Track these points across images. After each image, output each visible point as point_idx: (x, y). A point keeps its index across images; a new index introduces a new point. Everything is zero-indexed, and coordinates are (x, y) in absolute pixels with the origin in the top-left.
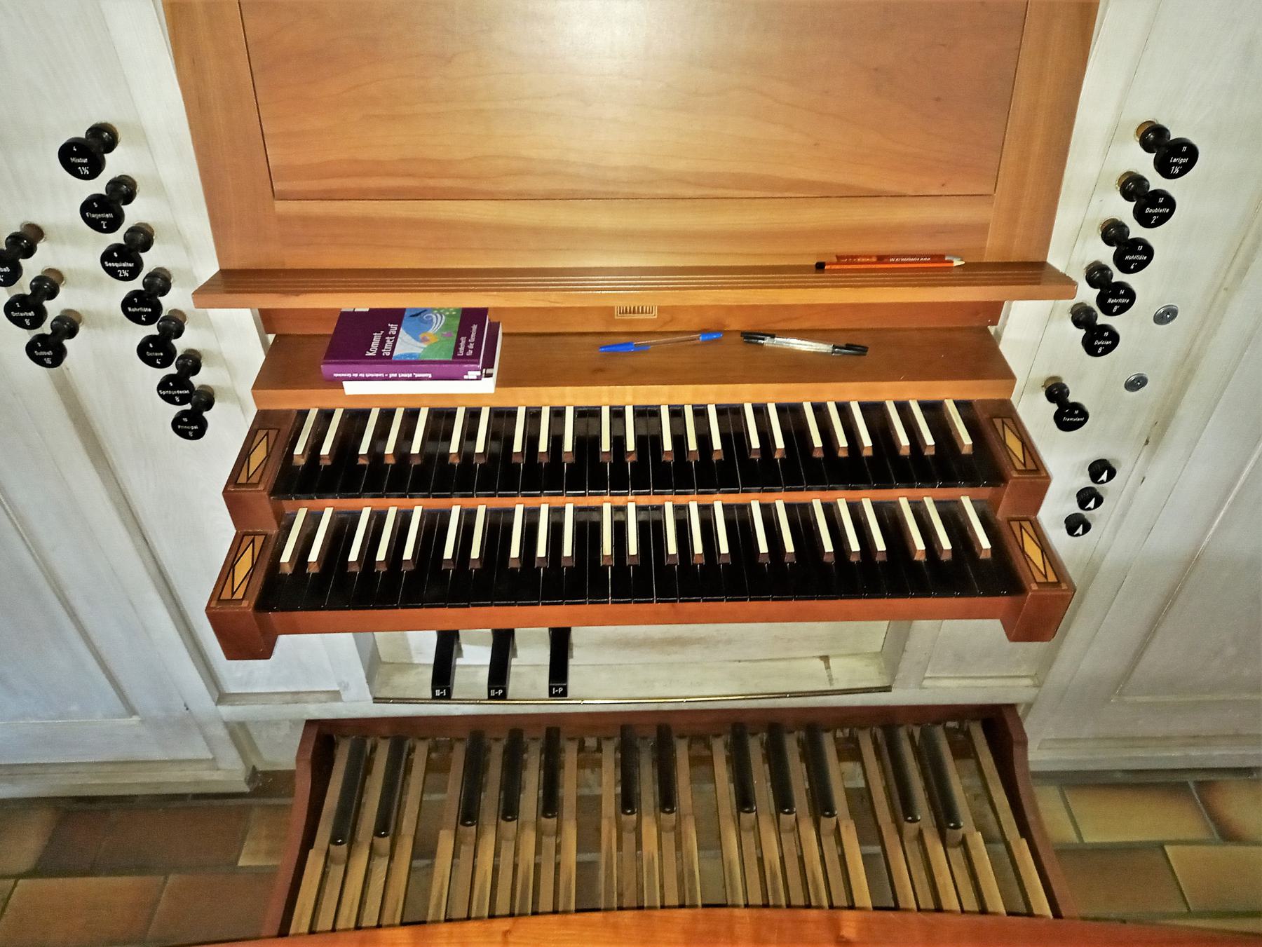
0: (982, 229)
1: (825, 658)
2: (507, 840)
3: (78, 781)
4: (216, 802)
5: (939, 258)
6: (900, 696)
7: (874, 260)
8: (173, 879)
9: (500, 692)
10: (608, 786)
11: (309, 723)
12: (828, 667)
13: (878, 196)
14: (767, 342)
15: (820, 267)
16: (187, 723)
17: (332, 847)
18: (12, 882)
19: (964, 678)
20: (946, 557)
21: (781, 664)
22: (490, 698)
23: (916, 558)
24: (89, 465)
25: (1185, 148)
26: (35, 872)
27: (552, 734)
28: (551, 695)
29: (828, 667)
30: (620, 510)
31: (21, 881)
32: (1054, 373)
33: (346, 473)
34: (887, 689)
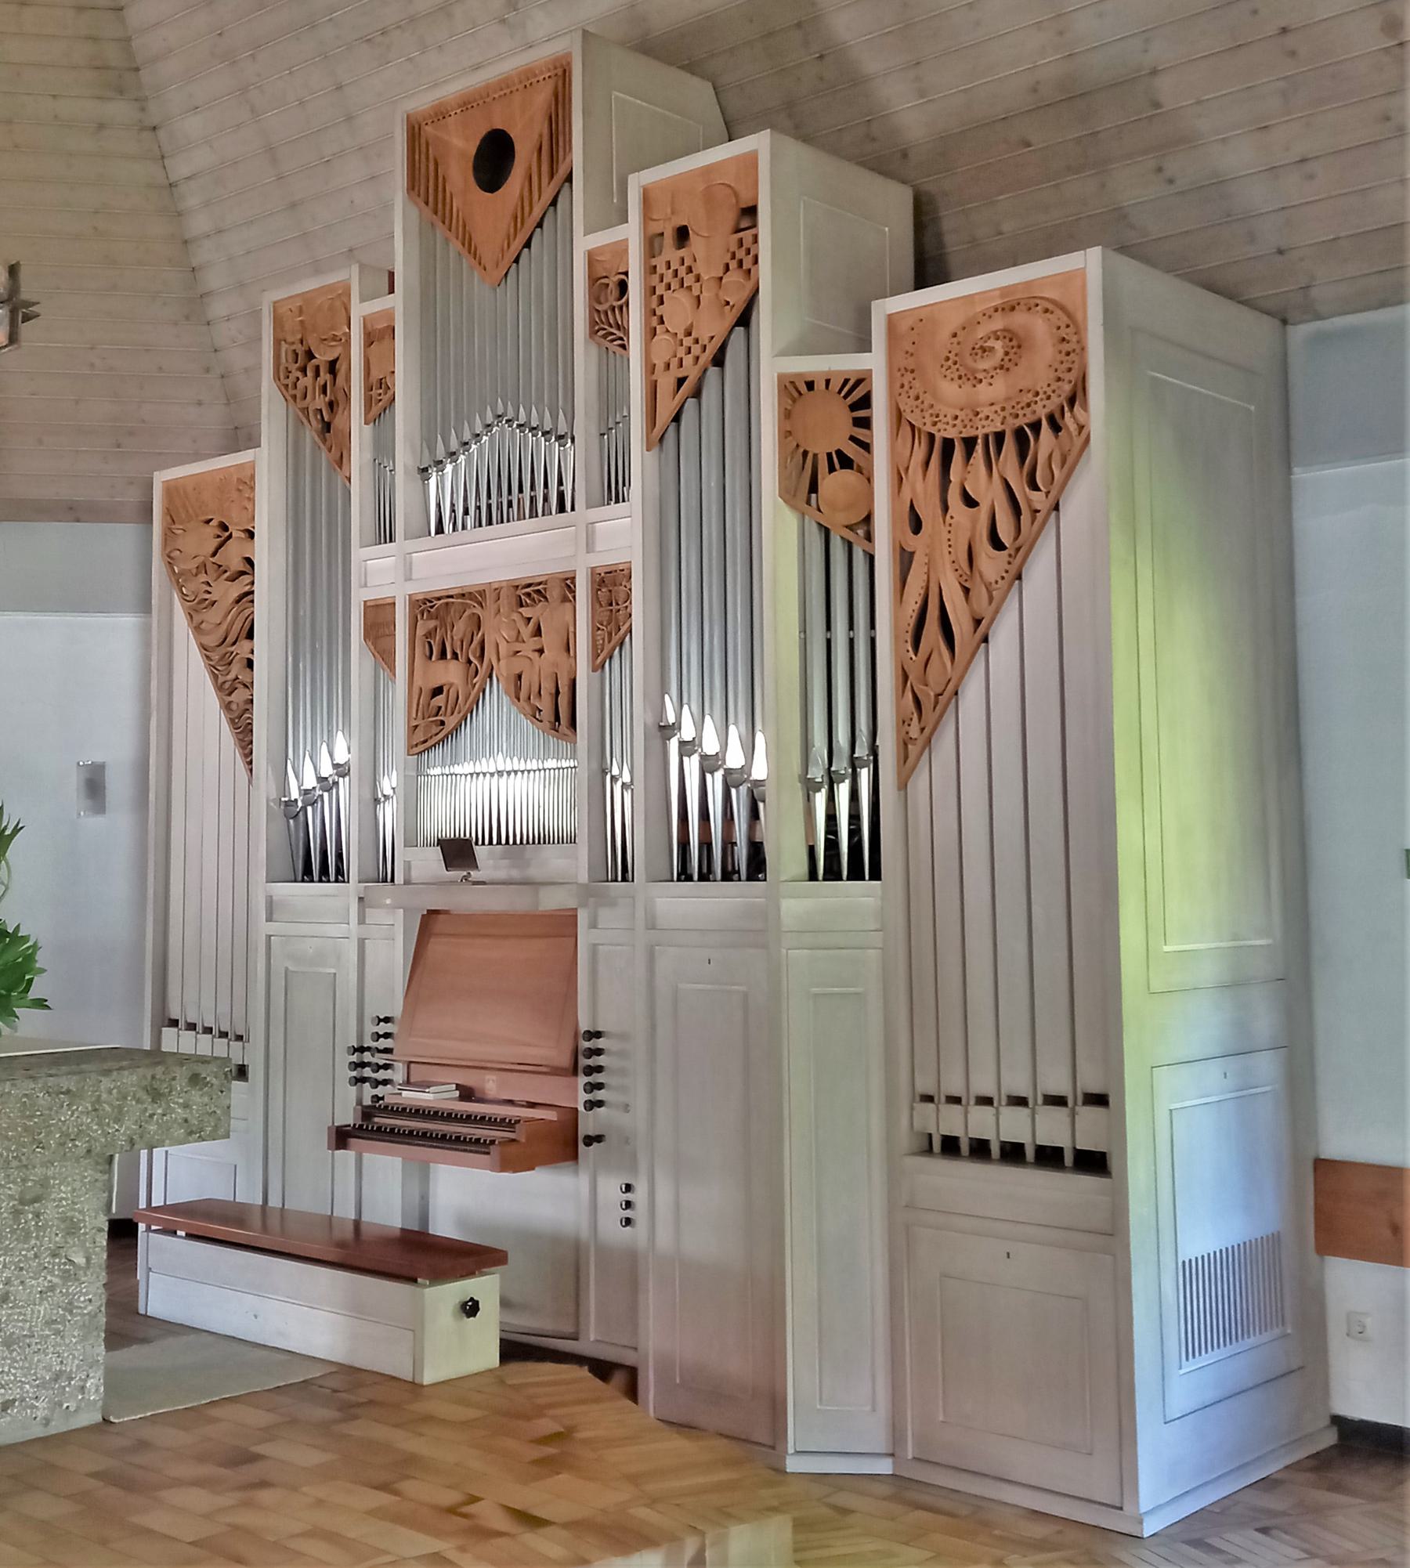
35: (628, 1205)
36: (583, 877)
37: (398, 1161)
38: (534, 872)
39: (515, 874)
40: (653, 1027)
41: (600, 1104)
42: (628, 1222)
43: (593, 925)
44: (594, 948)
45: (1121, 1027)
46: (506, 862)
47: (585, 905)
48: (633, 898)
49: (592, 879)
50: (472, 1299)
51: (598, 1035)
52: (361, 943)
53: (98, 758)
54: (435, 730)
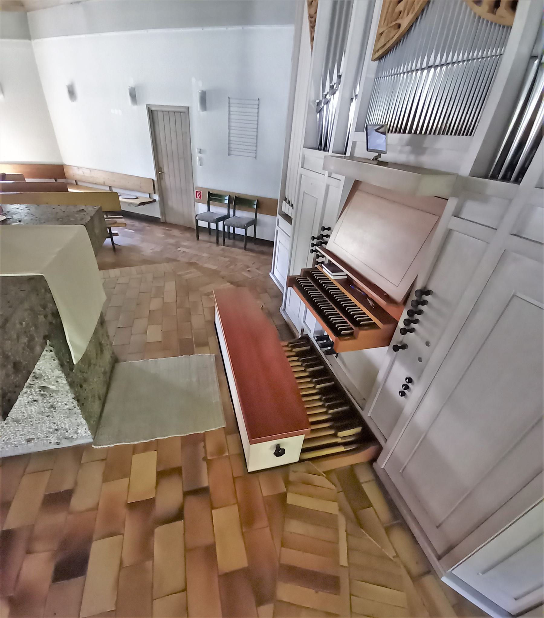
35: (407, 387)
36: (465, 169)
37: (122, 209)
38: (427, 160)
39: (411, 159)
40: (474, 311)
41: (412, 330)
42: (403, 394)
43: (457, 214)
44: (449, 233)
45: (51, 123)
46: (408, 148)
47: (455, 194)
48: (511, 200)
49: (473, 174)
50: (284, 450)
51: (428, 293)
52: (328, 187)
53: (331, 237)
54: (393, 32)
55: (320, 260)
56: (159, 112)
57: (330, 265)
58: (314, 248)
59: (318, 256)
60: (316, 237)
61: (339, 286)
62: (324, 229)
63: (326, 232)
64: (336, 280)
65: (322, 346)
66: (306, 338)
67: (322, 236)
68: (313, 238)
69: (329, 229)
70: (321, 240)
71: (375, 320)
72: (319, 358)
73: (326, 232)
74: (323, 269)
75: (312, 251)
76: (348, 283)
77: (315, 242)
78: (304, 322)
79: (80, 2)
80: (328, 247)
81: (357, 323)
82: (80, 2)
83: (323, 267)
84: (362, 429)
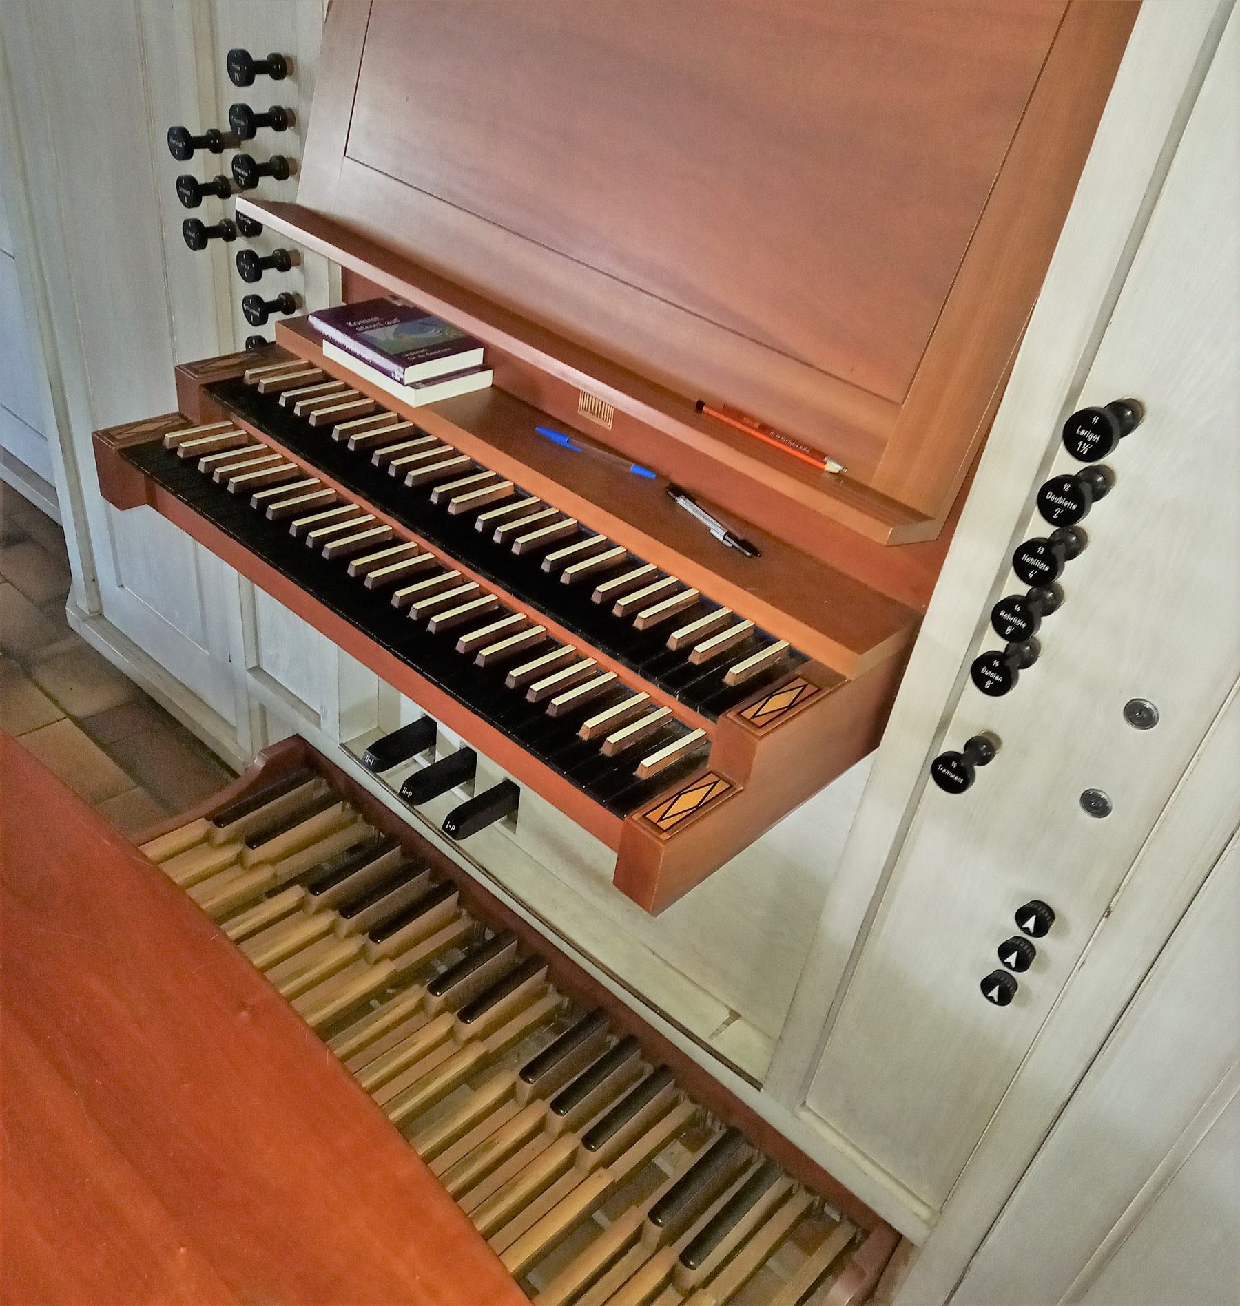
0: (879, 444)
1: (735, 1015)
2: (456, 1042)
3: (155, 682)
4: (219, 769)
5: (820, 455)
6: (767, 1105)
7: (757, 425)
8: (140, 790)
9: (453, 828)
10: (677, 1163)
11: (298, 737)
12: (727, 1023)
13: (811, 366)
14: (682, 501)
15: (700, 405)
16: (231, 682)
17: (649, 1223)
18: (63, 716)
19: (846, 1140)
20: (550, 712)
21: (686, 986)
22: (401, 795)
23: (579, 733)
24: (647, 683)
25: (1096, 420)
26: (78, 722)
27: (448, 881)
28: (444, 827)
29: (727, 1023)
30: (365, 517)
31: (67, 720)
32: (1001, 735)
33: (265, 410)
34: (757, 1085)
55: (271, 285)
56: (437, 1173)
57: (357, 313)
58: (210, 211)
59: (252, 267)
60: (196, 131)
61: (474, 449)
62: (244, 68)
63: (263, 94)
64: (437, 408)
65: (421, 789)
66: (299, 762)
67: (248, 122)
68: (184, 144)
69: (278, 67)
70: (240, 152)
71: (790, 633)
72: (417, 857)
73: (263, 94)
74: (329, 350)
75: (198, 235)
76: (514, 413)
77: (204, 166)
78: (257, 670)
79: (1109, 907)
80: (305, 191)
81: (707, 690)
82: (1109, 907)
83: (319, 337)
84: (404, 854)
